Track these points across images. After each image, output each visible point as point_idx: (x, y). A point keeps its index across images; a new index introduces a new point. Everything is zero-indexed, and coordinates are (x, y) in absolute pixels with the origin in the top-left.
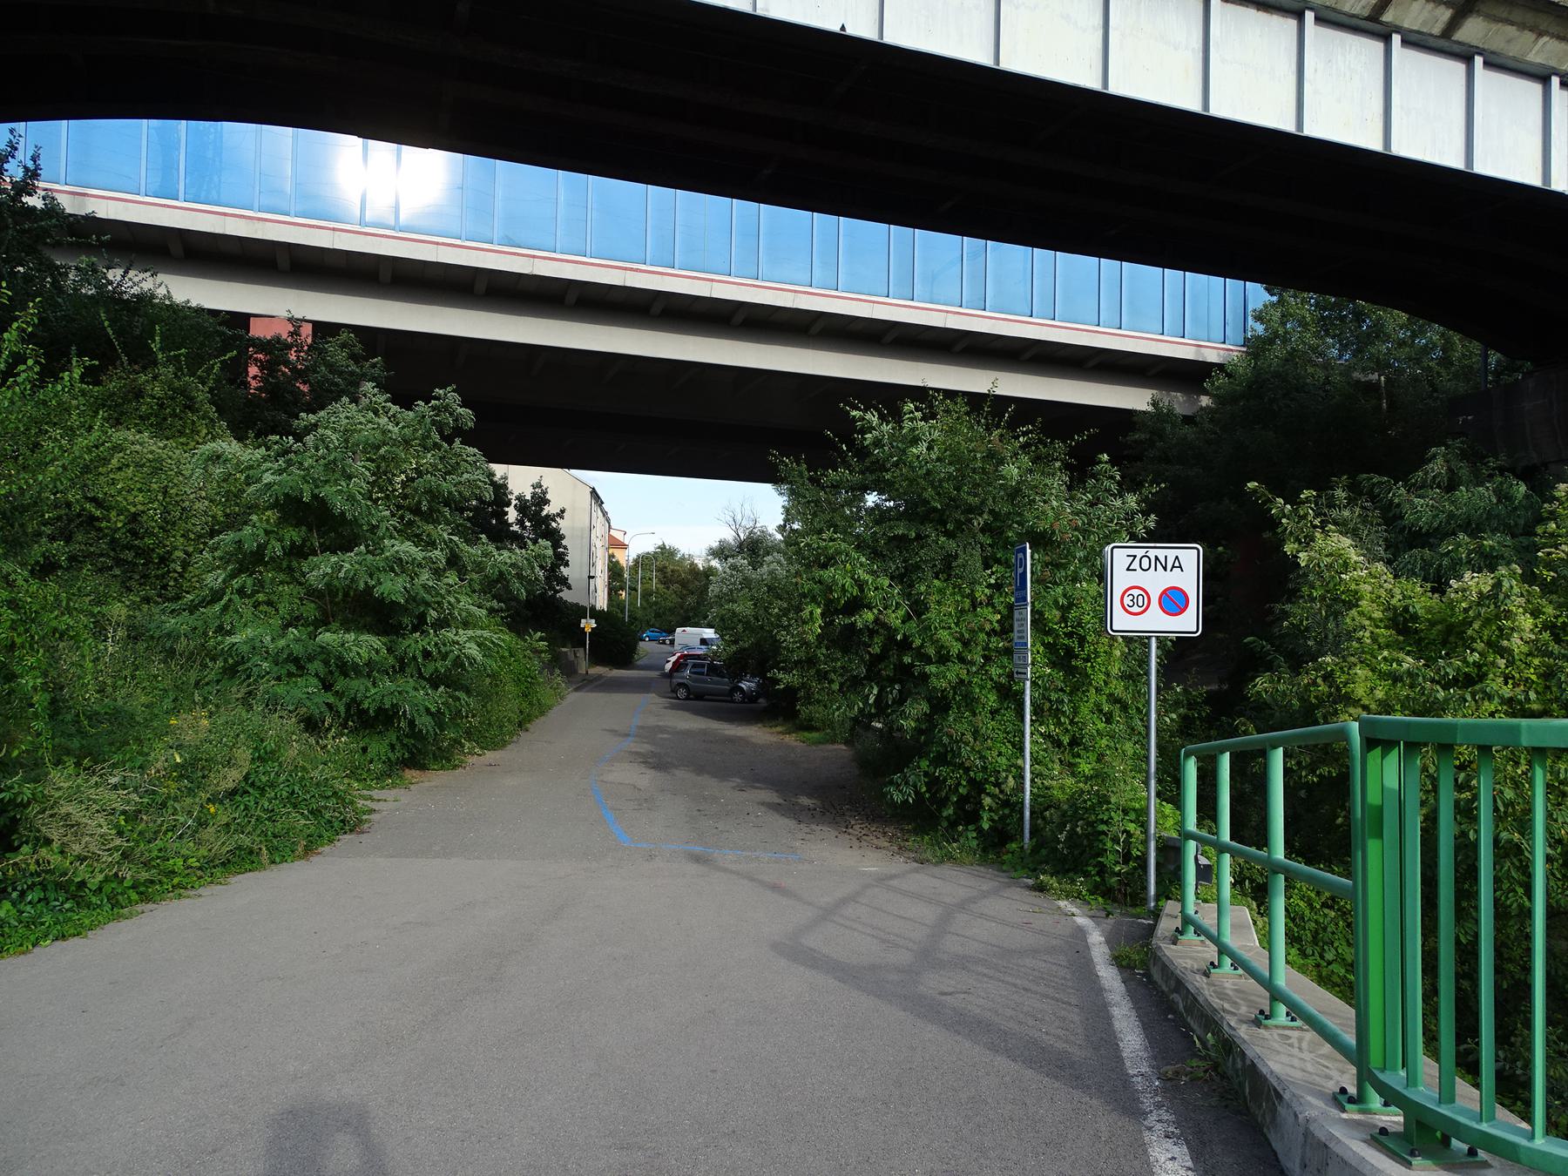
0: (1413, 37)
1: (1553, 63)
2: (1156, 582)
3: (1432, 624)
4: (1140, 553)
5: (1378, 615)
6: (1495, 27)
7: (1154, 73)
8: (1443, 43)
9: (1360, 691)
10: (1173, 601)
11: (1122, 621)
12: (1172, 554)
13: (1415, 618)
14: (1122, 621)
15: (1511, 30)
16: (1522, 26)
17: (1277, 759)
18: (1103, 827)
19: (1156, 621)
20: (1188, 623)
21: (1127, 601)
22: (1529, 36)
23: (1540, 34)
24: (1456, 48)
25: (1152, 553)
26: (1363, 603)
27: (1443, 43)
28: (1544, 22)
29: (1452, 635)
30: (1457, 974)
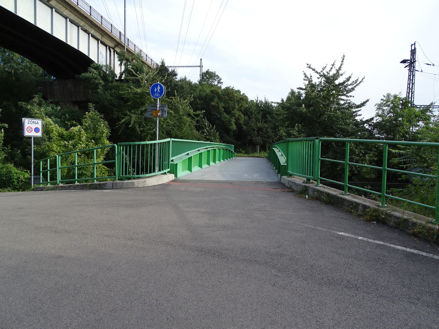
0: (57, 10)
1: (68, 16)
2: (34, 126)
3: (67, 136)
4: (30, 120)
5: (57, 134)
6: (58, 4)
7: (25, 13)
8: (47, 3)
9: (55, 149)
10: (37, 130)
11: (27, 134)
12: (36, 121)
13: (64, 135)
14: (27, 134)
15: (61, 6)
16: (63, 6)
17: (49, 160)
18: (12, 177)
19: (33, 134)
20: (39, 134)
21: (28, 129)
22: (64, 9)
23: (66, 9)
24: (49, 5)
25: (33, 120)
26: (54, 132)
27: (47, 3)
28: (62, 3)
29: (71, 137)
30: (83, 188)
